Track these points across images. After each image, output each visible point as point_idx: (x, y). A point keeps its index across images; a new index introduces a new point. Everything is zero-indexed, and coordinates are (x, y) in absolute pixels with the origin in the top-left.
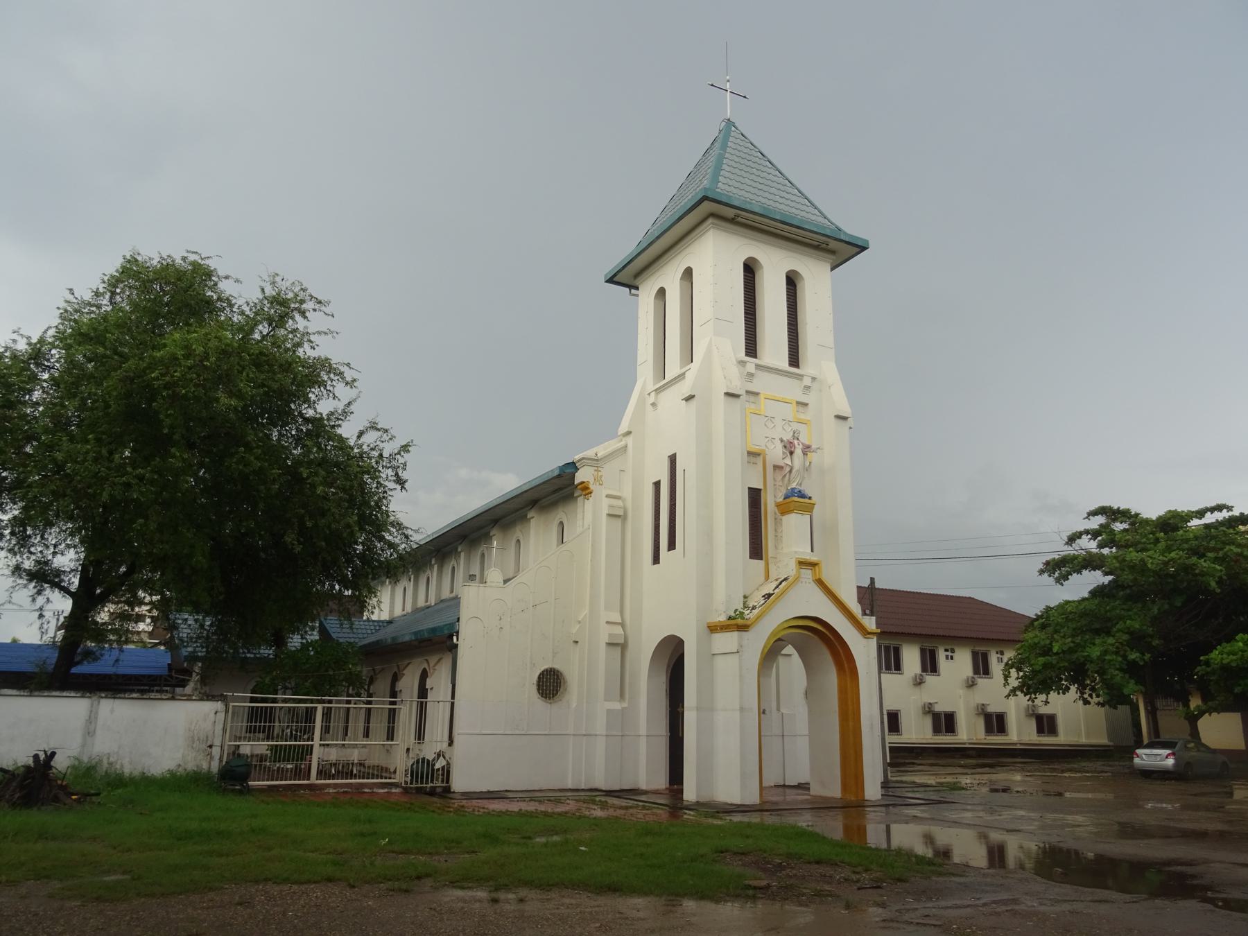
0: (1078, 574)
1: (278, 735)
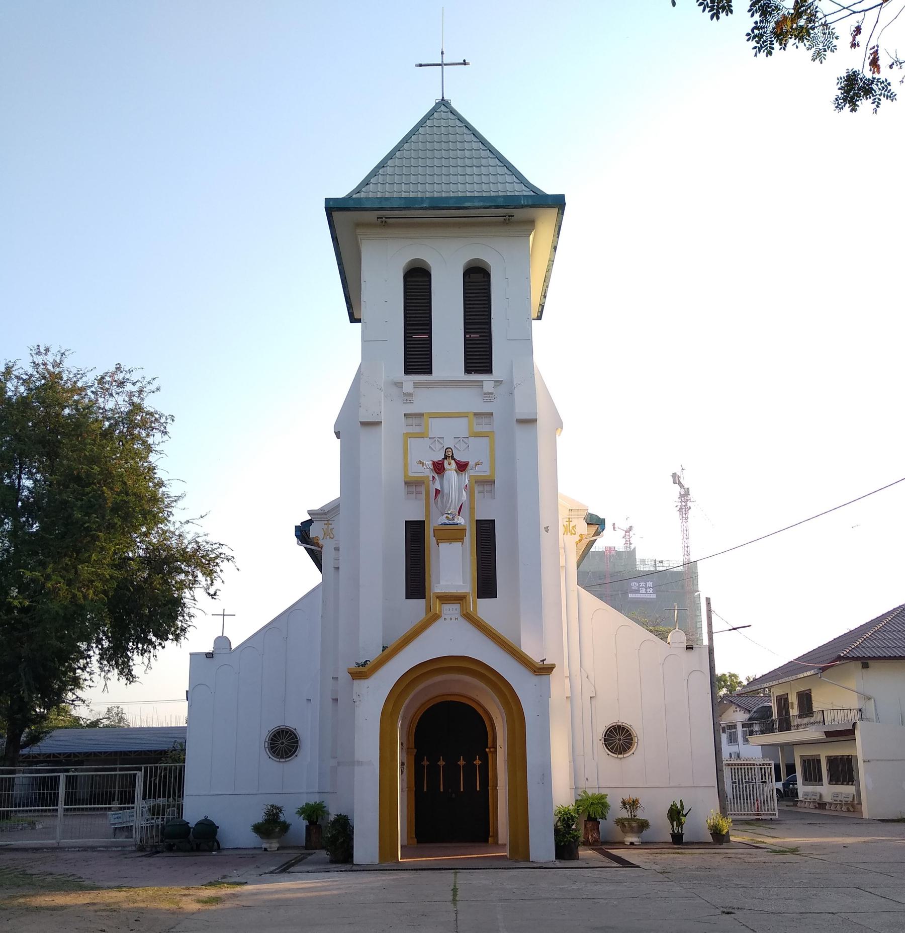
0: (341, 815)
1: (20, 803)
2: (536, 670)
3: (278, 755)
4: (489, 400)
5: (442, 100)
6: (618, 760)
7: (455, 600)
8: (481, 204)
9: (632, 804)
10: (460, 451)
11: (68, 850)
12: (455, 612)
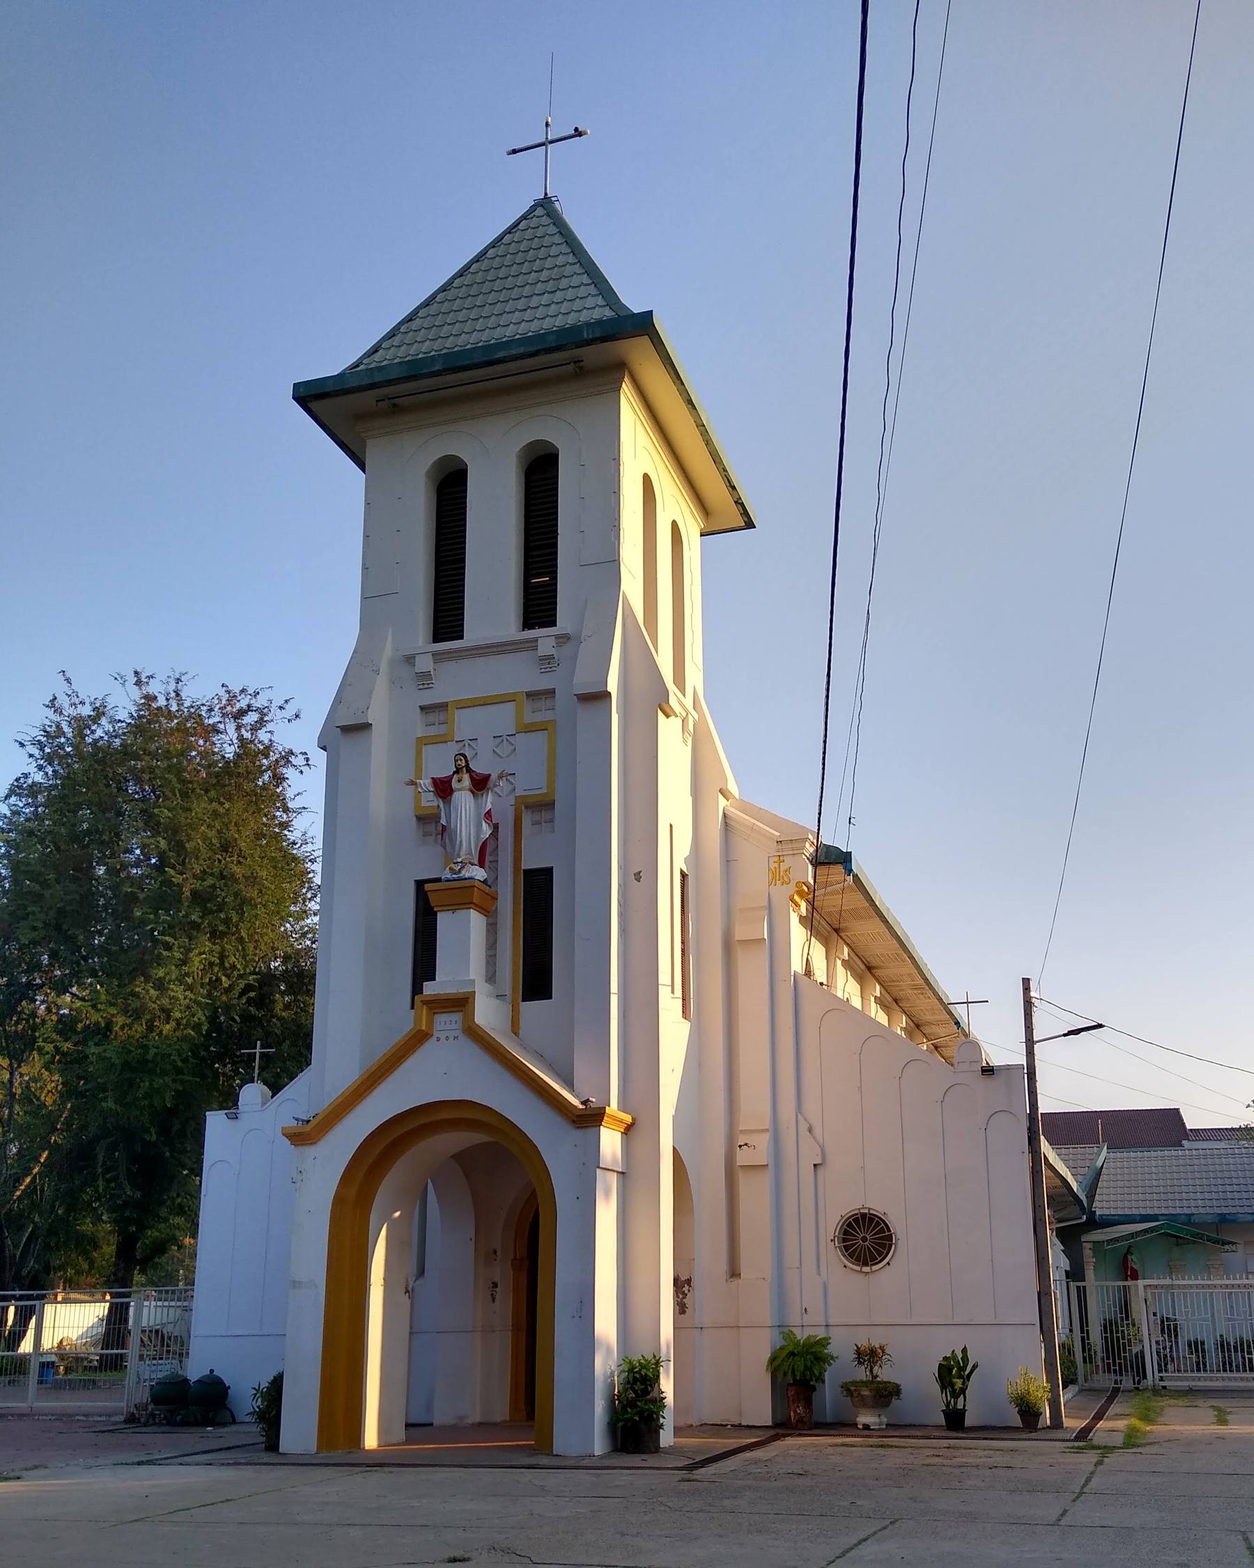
2: (575, 1119)
3: (858, 1259)
4: (549, 669)
5: (545, 198)
6: (861, 1276)
7: (455, 1006)
8: (522, 350)
9: (869, 1356)
10: (501, 757)
11: (39, 1419)
12: (454, 1026)
